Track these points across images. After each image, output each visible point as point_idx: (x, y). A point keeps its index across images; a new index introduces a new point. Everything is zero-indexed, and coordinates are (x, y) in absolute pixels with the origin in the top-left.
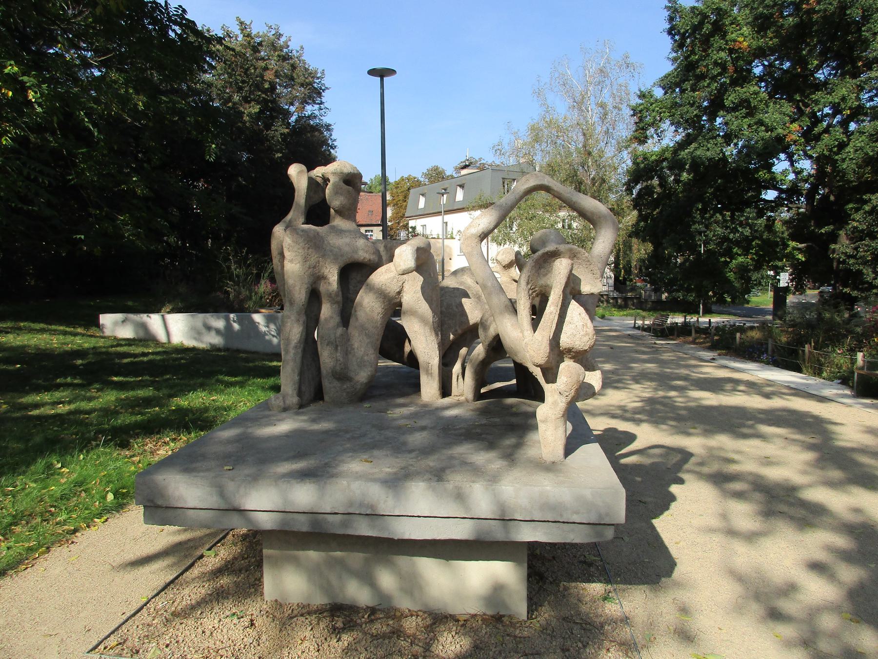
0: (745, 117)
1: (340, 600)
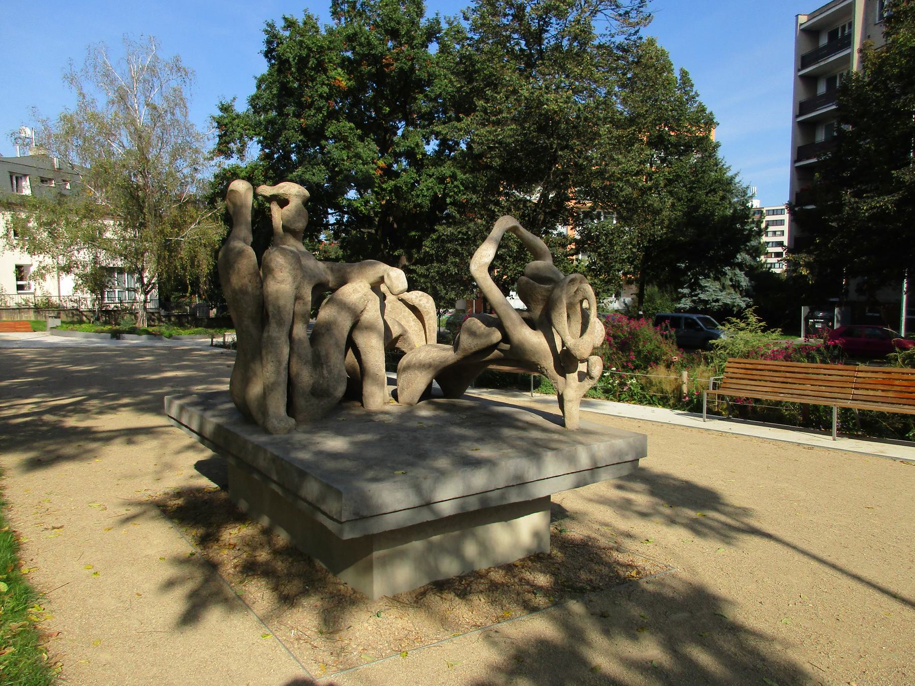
0: (343, 149)
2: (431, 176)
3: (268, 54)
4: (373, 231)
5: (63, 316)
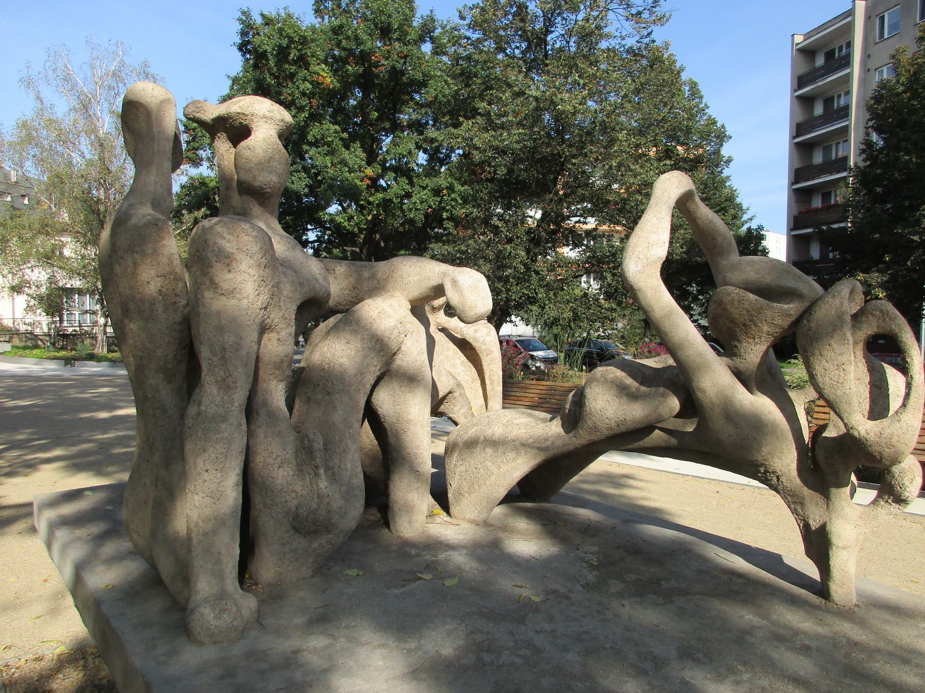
0: (327, 155)
2: (424, 188)
3: (243, 47)
4: (358, 250)
5: (16, 341)
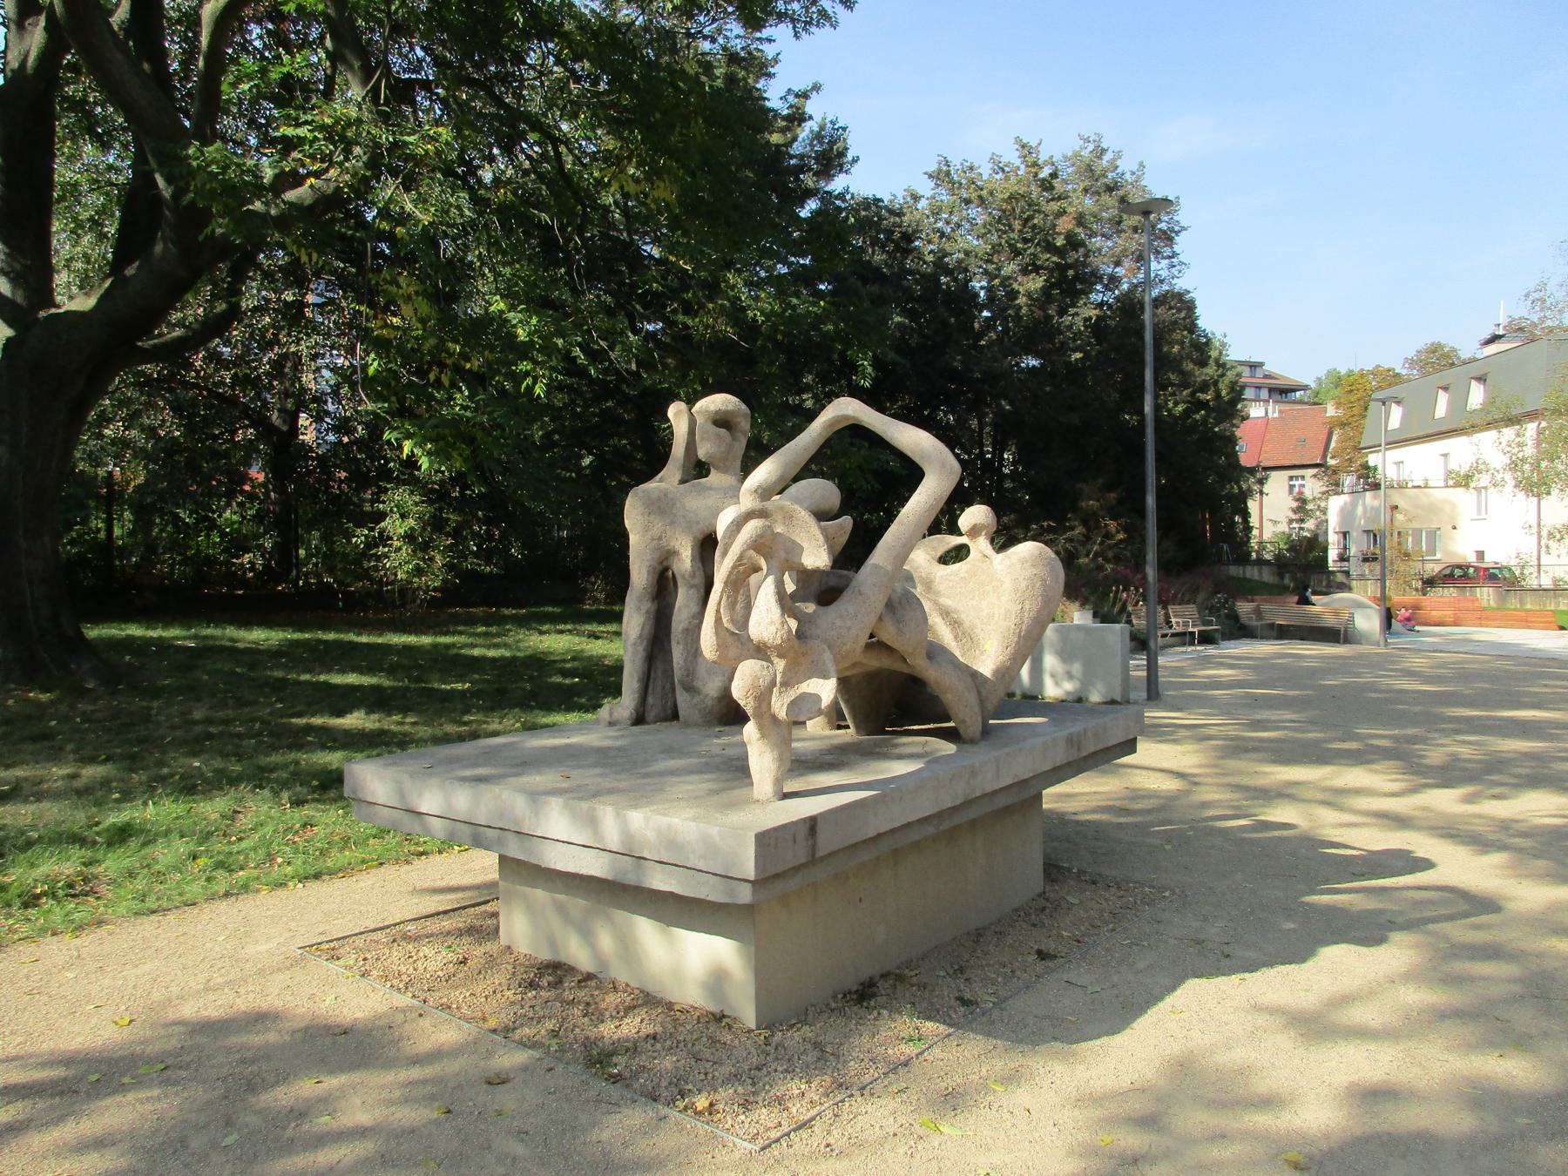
1: (563, 958)
